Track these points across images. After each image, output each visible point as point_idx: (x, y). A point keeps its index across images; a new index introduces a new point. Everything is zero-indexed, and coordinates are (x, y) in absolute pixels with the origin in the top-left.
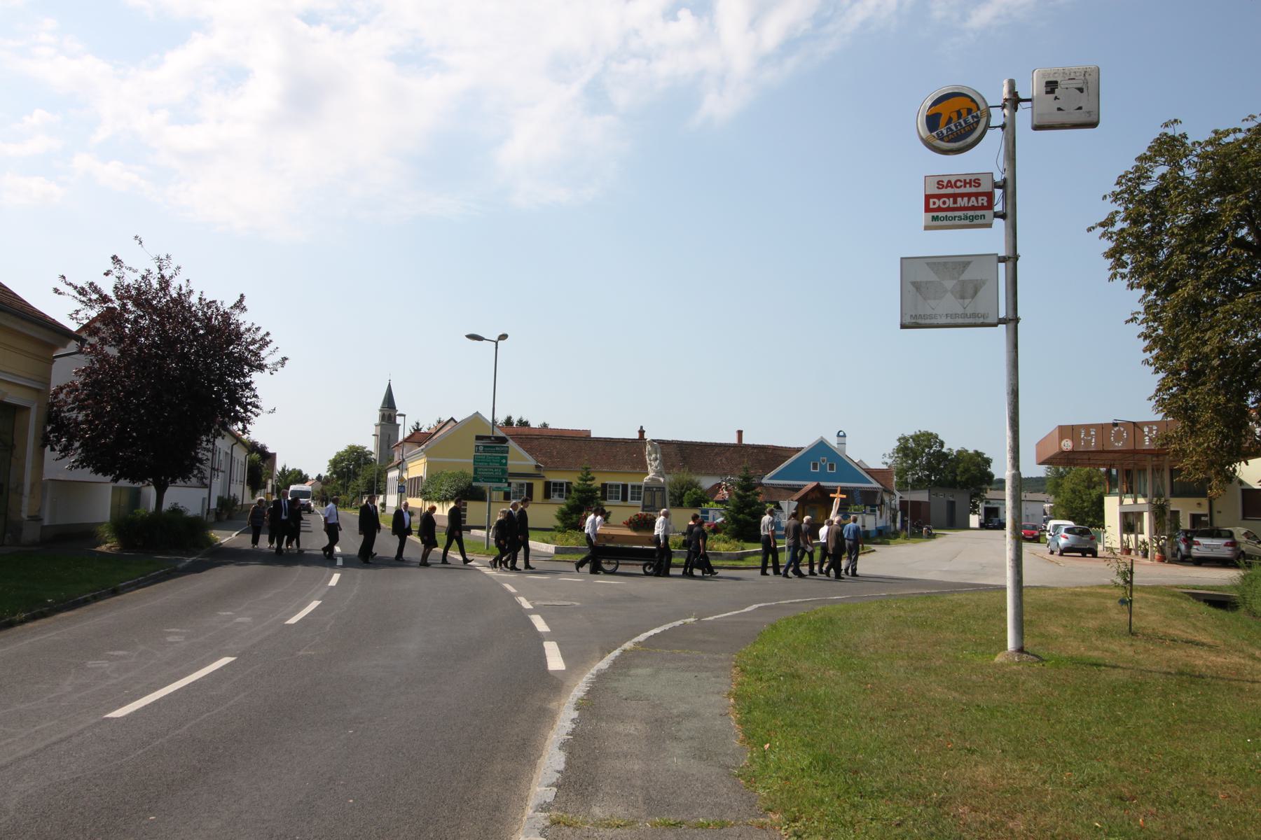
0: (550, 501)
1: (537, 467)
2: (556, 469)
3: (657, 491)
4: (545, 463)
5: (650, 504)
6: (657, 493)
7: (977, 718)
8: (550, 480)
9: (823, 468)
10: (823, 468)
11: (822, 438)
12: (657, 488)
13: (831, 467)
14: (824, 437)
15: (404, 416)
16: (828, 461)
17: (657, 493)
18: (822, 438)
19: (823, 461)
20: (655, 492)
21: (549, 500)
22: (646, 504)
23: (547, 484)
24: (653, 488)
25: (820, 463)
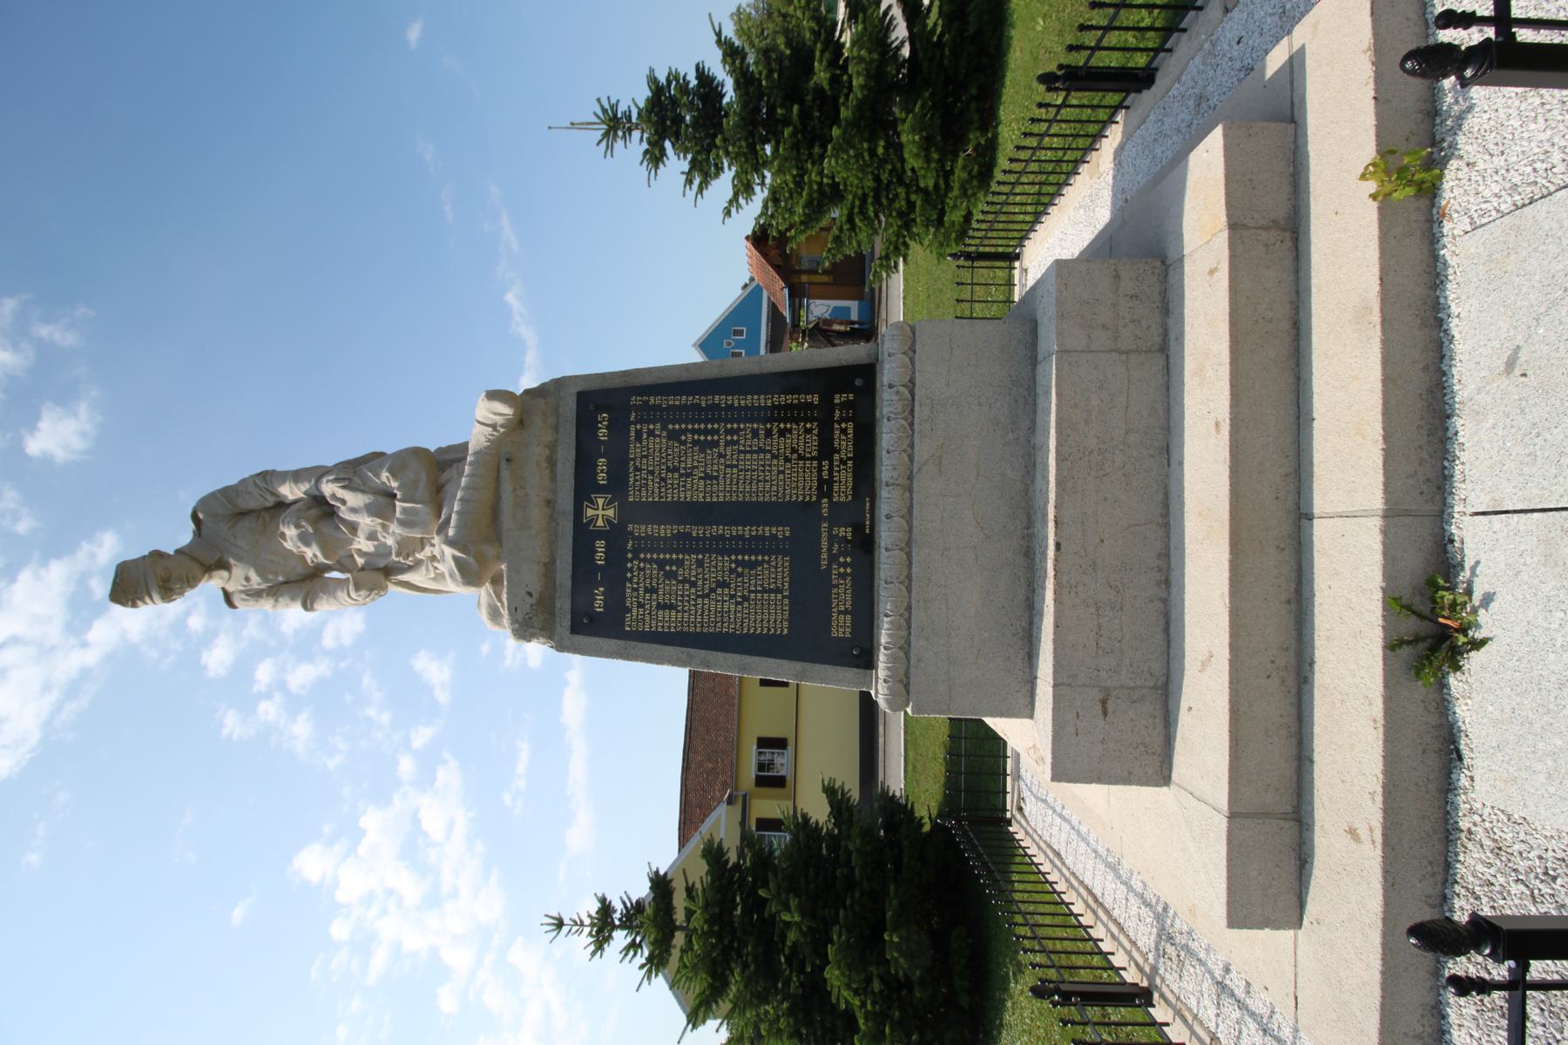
0: (790, 778)
1: (730, 801)
2: (735, 768)
3: (617, 487)
4: (725, 785)
5: (777, 570)
6: (644, 490)
7: (1446, 120)
8: (753, 776)
9: (739, 344)
10: (739, 344)
11: (694, 345)
12: (584, 489)
13: (740, 333)
14: (693, 341)
15: (957, 317)
16: (729, 338)
17: (644, 490)
18: (694, 345)
19: (729, 344)
20: (629, 512)
21: (788, 778)
22: (774, 617)
23: (762, 782)
24: (583, 534)
25: (733, 348)
